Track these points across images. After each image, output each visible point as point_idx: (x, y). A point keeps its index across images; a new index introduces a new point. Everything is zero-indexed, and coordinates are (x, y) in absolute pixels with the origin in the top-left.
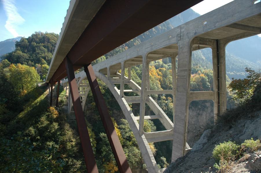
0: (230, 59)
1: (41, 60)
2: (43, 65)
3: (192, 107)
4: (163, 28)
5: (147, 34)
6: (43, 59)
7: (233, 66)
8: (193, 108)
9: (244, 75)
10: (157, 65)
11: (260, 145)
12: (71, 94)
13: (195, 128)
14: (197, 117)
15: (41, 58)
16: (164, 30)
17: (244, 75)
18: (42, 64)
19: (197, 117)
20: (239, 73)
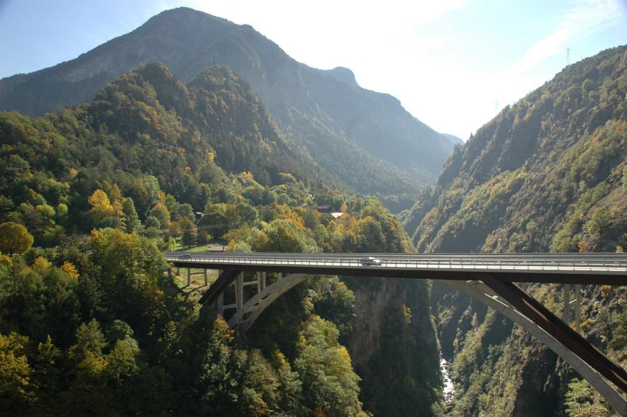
0: (366, 165)
1: (28, 191)
2: (40, 207)
3: (359, 285)
4: (240, 98)
5: (212, 114)
6: (31, 190)
7: (375, 182)
8: (362, 287)
9: (398, 202)
10: (250, 190)
11: (624, 43)
12: (576, 264)
13: (364, 327)
14: (369, 304)
15: (26, 186)
16: (242, 102)
17: (398, 202)
18: (35, 203)
19: (369, 304)
20: (387, 197)
